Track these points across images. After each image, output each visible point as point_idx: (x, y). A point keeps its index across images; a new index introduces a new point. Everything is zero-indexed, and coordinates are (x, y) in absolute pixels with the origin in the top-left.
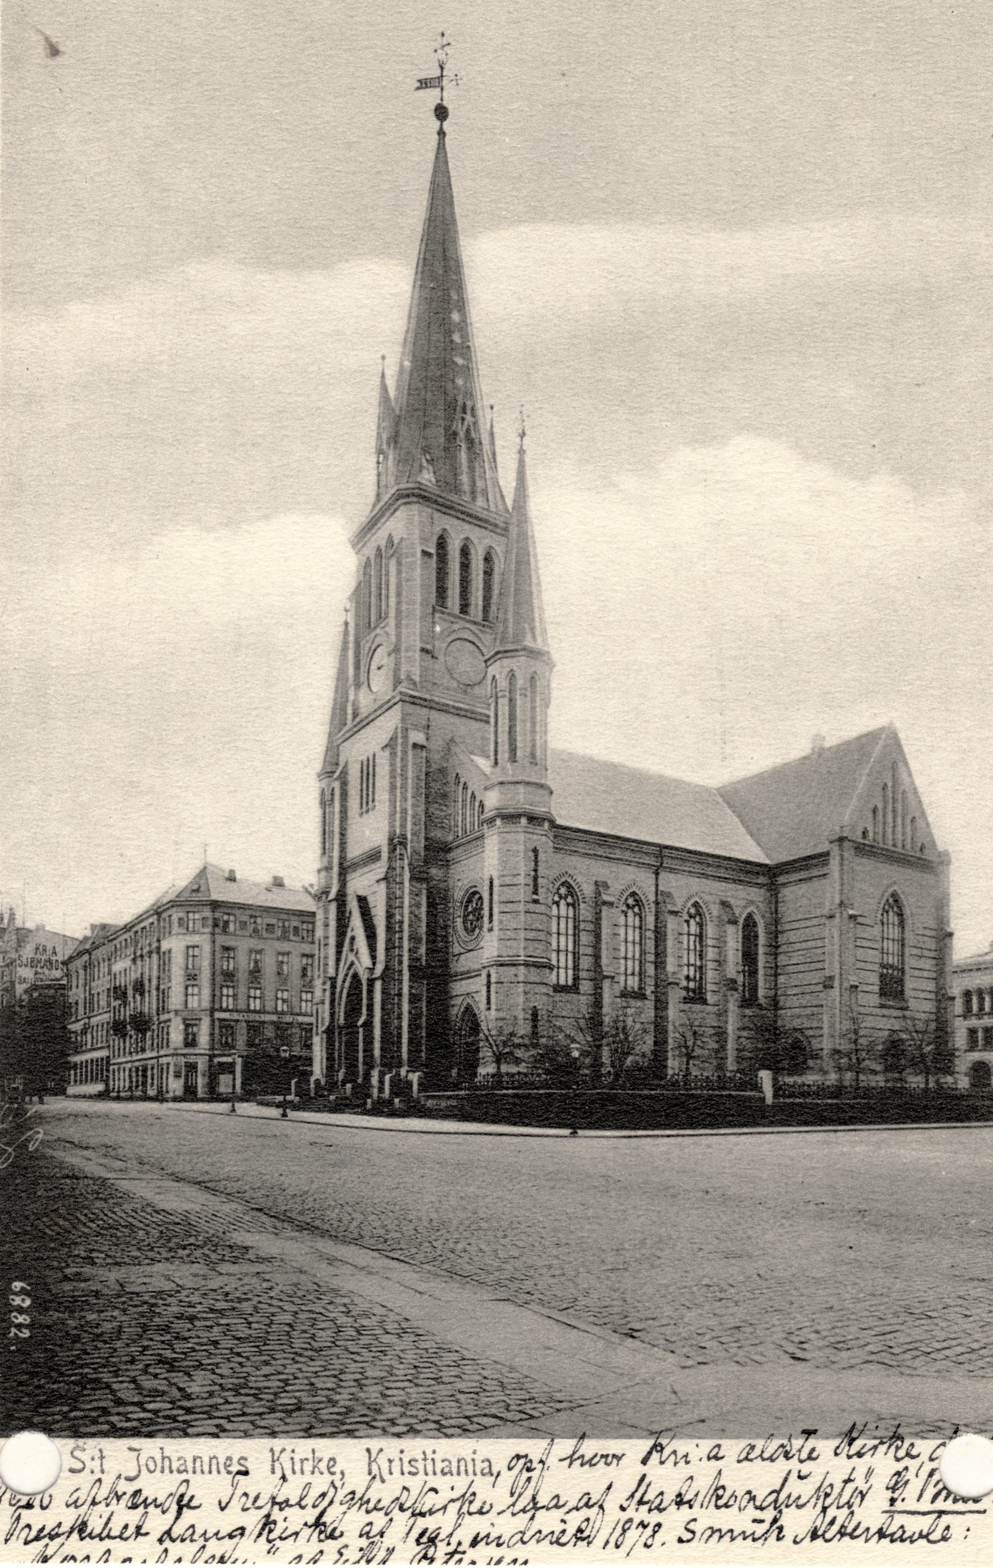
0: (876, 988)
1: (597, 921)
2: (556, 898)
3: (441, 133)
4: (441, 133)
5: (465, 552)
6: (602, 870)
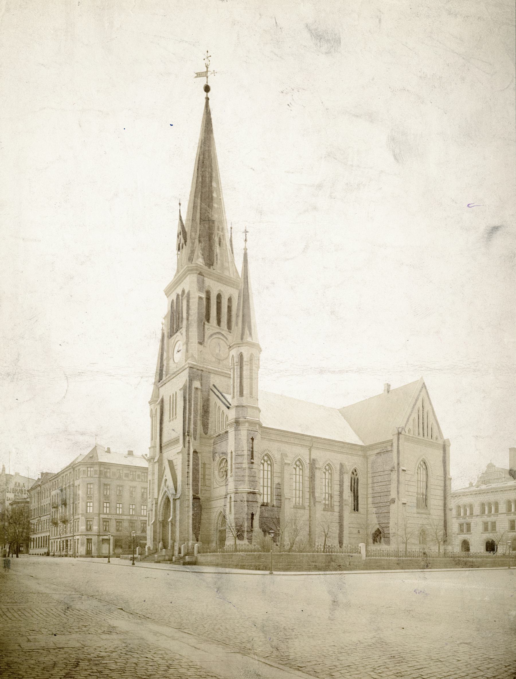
0: (415, 505)
1: (282, 472)
2: (263, 462)
3: (207, 99)
4: (207, 99)
5: (219, 297)
6: (286, 448)
